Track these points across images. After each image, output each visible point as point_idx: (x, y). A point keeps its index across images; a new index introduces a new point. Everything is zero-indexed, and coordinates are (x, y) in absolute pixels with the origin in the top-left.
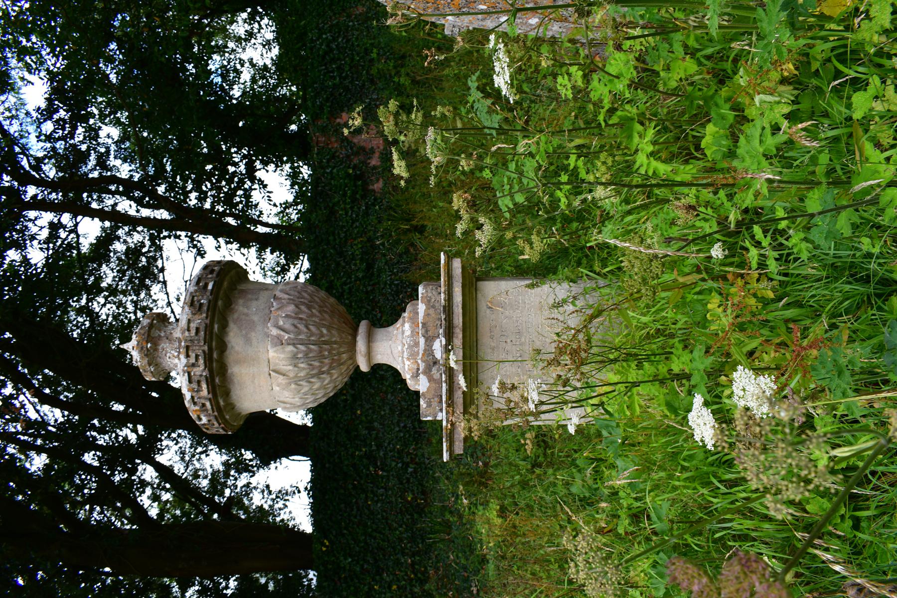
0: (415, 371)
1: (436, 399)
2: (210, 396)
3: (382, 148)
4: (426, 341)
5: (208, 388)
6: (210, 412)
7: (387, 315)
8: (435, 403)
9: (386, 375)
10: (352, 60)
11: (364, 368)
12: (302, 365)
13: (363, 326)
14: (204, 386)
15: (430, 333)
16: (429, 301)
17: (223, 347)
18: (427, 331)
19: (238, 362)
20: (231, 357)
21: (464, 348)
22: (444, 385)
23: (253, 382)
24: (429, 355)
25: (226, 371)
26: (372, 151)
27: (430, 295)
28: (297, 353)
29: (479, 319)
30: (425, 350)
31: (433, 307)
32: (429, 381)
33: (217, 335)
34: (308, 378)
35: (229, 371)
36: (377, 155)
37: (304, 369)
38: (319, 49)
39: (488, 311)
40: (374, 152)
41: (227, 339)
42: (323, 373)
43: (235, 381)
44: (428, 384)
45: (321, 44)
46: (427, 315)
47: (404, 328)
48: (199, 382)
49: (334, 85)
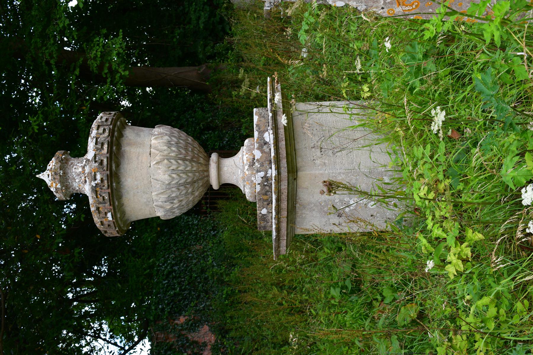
0: (251, 160)
1: (267, 162)
2: (108, 155)
3: (213, 342)
4: (259, 133)
5: (108, 148)
6: (105, 168)
7: (229, 150)
8: (266, 164)
9: (230, 191)
10: (191, 277)
11: (215, 186)
12: (174, 149)
13: (214, 157)
14: (106, 146)
15: (261, 129)
16: (261, 114)
17: (121, 135)
18: (259, 129)
19: (129, 144)
20: (125, 141)
21: (288, 201)
22: (274, 221)
23: (138, 158)
24: (261, 140)
25: (121, 149)
26: (205, 344)
27: (261, 111)
28: (171, 141)
29: (296, 136)
30: (258, 138)
31: (263, 117)
32: (262, 153)
33: (118, 127)
34: (176, 159)
35: (123, 149)
36: (209, 347)
37: (174, 151)
38: (164, 271)
39: (302, 134)
40: (206, 345)
41: (123, 133)
42: (187, 160)
43: (126, 156)
44: (261, 155)
45: (166, 267)
46: (259, 120)
47: (243, 156)
48: (103, 144)
49: (175, 293)
